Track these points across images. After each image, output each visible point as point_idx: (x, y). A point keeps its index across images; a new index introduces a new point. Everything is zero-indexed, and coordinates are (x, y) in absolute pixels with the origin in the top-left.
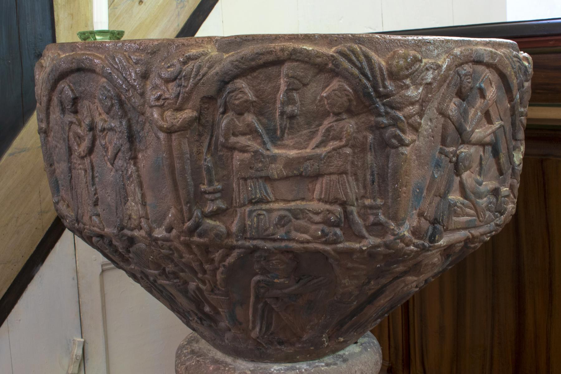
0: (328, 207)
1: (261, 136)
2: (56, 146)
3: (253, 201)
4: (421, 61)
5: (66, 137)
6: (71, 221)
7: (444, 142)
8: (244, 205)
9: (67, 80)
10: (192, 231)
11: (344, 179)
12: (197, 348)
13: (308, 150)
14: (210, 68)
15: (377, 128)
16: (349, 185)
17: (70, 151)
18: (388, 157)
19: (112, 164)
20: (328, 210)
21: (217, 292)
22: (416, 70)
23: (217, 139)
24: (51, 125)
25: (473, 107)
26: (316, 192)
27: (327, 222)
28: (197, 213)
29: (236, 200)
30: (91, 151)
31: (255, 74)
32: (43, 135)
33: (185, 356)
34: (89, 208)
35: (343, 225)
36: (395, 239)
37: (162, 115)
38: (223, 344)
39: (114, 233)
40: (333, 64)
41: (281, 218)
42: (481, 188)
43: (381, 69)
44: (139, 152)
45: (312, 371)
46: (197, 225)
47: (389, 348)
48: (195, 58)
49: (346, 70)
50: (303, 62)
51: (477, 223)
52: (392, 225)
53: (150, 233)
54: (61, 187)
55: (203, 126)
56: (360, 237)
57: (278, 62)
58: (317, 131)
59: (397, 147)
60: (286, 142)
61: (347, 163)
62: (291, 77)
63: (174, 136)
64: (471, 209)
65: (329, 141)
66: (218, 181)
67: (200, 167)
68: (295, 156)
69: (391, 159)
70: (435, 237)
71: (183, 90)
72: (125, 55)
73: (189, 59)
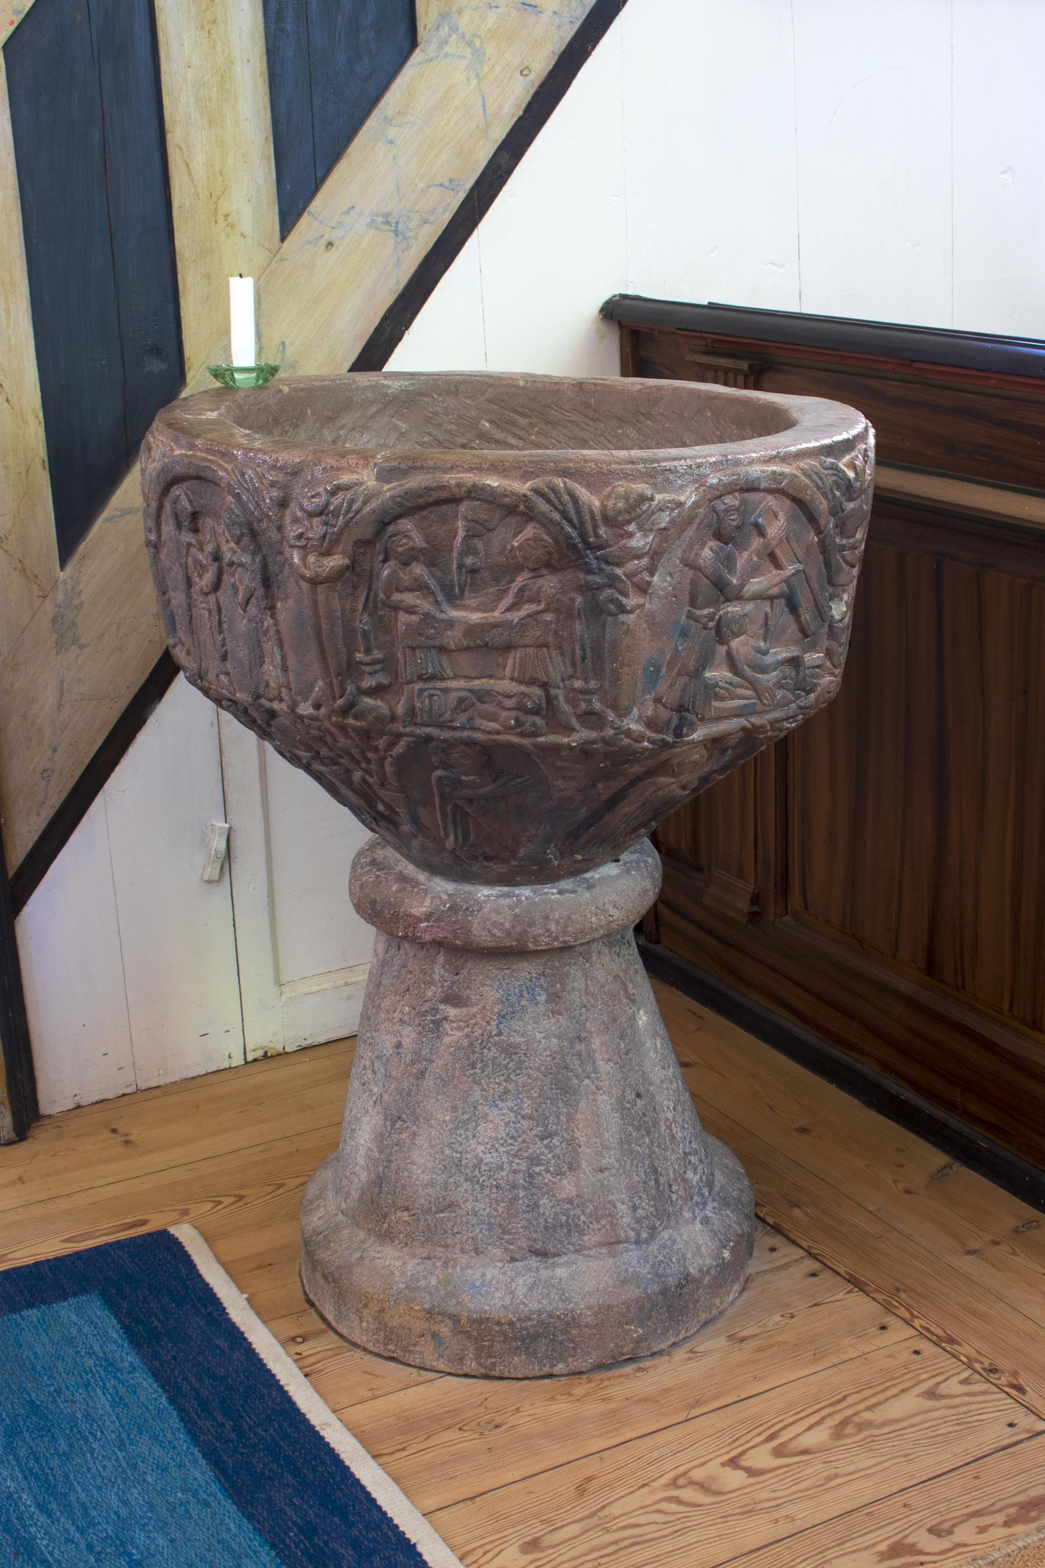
0: (523, 688)
1: (433, 593)
2: (171, 568)
3: (424, 677)
4: (652, 499)
5: (183, 561)
6: (193, 676)
7: (693, 602)
8: (412, 682)
9: (185, 485)
10: (345, 711)
11: (544, 654)
12: (382, 856)
13: (496, 614)
14: (365, 503)
15: (585, 589)
16: (552, 661)
17: (189, 583)
18: (604, 626)
19: (245, 611)
20: (523, 693)
21: (389, 787)
22: (644, 512)
23: (376, 595)
24: (163, 538)
25: (746, 550)
26: (507, 668)
27: (521, 708)
28: (350, 688)
29: (401, 674)
30: (216, 586)
31: (425, 513)
32: (153, 550)
33: (362, 868)
34: (216, 663)
35: (544, 712)
36: (616, 734)
37: (304, 559)
38: (411, 854)
39: (247, 701)
40: (525, 506)
41: (461, 700)
42: (766, 658)
43: (592, 513)
44: (278, 599)
45: (536, 899)
46: (351, 705)
47: (756, 862)
48: (346, 488)
49: (543, 514)
50: (486, 501)
51: (760, 707)
52: (611, 716)
53: (293, 708)
54: (178, 625)
55: (358, 575)
56: (570, 730)
57: (454, 500)
58: (508, 589)
59: (615, 615)
60: (467, 602)
61: (548, 633)
62: (471, 520)
63: (320, 589)
64: (747, 688)
65: (524, 603)
66: (379, 648)
67: (354, 630)
68: (478, 621)
69: (608, 630)
70: (682, 730)
71: (330, 530)
72: (257, 473)
73: (338, 489)
